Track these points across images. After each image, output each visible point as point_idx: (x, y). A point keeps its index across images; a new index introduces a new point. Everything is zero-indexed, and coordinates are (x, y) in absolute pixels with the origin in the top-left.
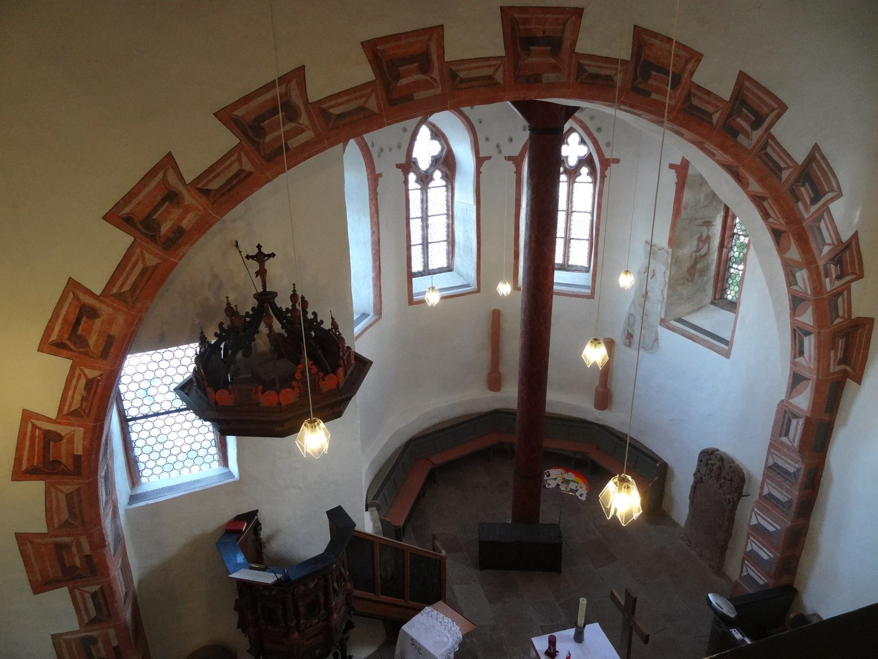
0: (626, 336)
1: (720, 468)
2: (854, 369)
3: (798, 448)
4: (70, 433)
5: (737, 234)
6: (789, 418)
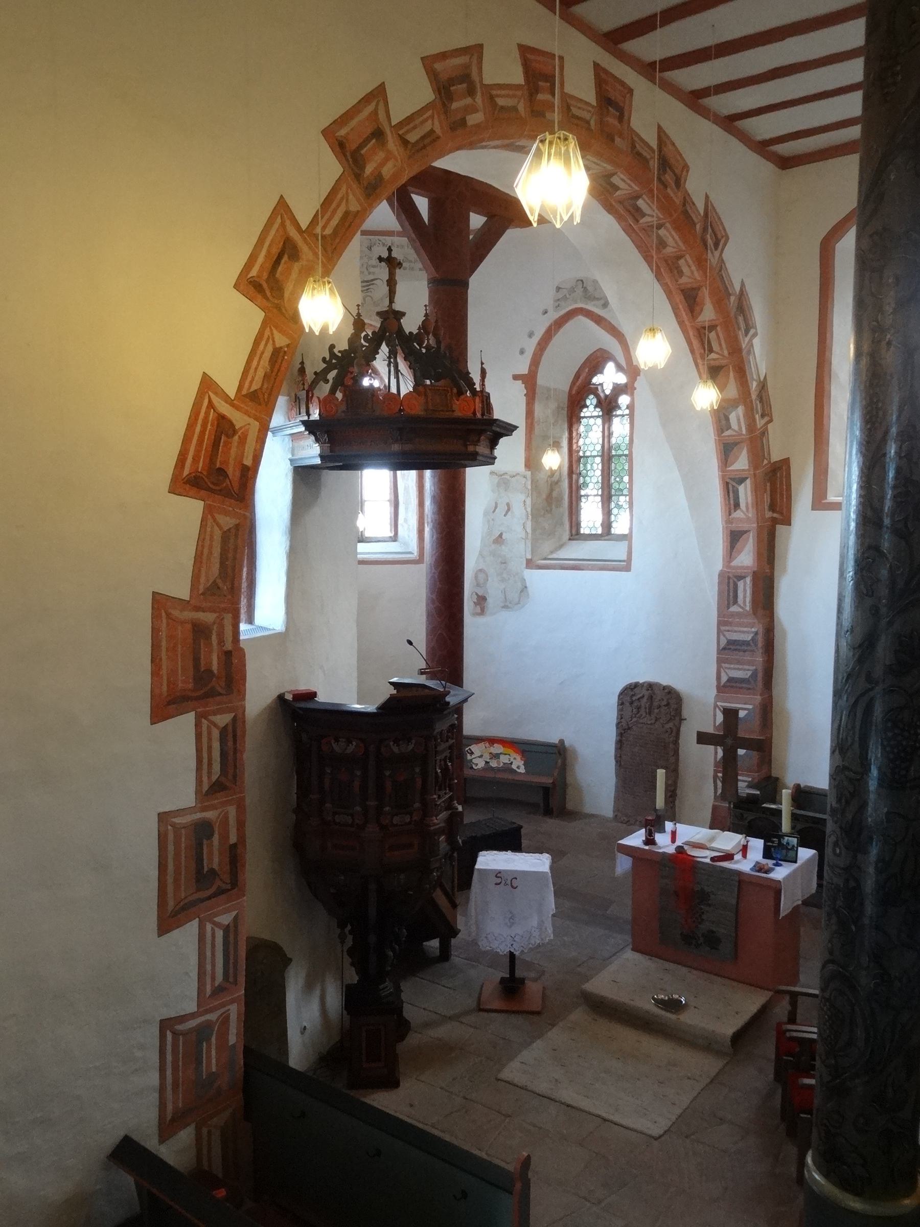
0: (474, 602)
1: (651, 698)
2: (782, 514)
3: (751, 610)
4: (244, 426)
5: (584, 457)
6: (734, 581)
